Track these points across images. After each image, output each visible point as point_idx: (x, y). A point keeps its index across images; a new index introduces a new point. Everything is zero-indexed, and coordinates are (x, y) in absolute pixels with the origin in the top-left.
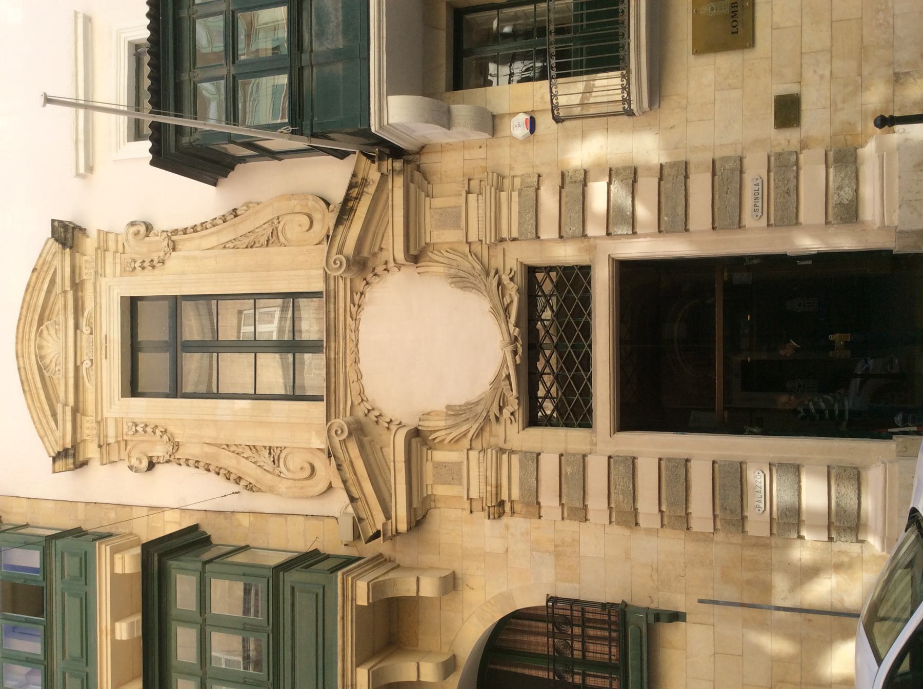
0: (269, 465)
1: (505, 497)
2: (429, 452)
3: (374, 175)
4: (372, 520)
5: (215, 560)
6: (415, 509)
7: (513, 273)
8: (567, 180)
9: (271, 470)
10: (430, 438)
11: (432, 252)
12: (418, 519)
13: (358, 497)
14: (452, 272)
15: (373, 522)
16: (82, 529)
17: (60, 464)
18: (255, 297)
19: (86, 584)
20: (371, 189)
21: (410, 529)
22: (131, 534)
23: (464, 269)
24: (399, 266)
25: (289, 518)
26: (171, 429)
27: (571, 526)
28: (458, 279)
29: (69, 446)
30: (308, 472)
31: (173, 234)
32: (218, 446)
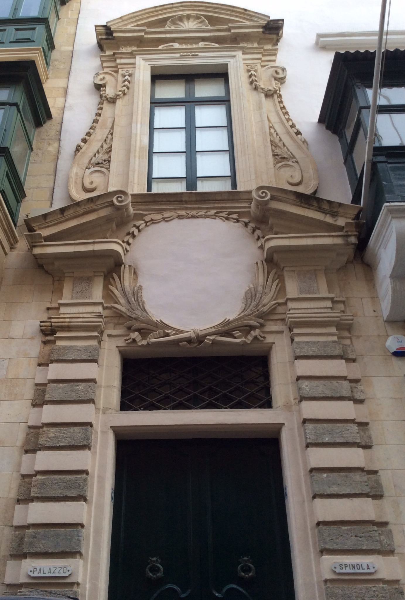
0: (94, 160)
1: (58, 335)
2: (102, 274)
3: (341, 222)
4: (44, 226)
5: (19, 113)
6: (53, 263)
7: (261, 339)
8: (353, 385)
9: (92, 162)
10: (114, 274)
11: (276, 273)
12: (44, 266)
13: (65, 215)
14: (259, 288)
15: (42, 226)
16: (53, 49)
17: (102, 30)
18: (231, 151)
19: (11, 42)
20: (329, 219)
21: (34, 255)
22: (47, 78)
23: (263, 298)
24: (261, 247)
25: (52, 177)
26: (126, 97)
27: (29, 393)
28: (254, 293)
29: (115, 35)
30: (88, 185)
31: (278, 95)
32: (112, 127)
